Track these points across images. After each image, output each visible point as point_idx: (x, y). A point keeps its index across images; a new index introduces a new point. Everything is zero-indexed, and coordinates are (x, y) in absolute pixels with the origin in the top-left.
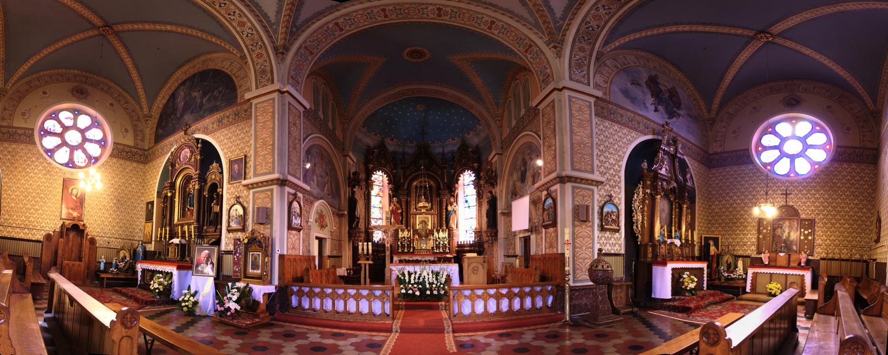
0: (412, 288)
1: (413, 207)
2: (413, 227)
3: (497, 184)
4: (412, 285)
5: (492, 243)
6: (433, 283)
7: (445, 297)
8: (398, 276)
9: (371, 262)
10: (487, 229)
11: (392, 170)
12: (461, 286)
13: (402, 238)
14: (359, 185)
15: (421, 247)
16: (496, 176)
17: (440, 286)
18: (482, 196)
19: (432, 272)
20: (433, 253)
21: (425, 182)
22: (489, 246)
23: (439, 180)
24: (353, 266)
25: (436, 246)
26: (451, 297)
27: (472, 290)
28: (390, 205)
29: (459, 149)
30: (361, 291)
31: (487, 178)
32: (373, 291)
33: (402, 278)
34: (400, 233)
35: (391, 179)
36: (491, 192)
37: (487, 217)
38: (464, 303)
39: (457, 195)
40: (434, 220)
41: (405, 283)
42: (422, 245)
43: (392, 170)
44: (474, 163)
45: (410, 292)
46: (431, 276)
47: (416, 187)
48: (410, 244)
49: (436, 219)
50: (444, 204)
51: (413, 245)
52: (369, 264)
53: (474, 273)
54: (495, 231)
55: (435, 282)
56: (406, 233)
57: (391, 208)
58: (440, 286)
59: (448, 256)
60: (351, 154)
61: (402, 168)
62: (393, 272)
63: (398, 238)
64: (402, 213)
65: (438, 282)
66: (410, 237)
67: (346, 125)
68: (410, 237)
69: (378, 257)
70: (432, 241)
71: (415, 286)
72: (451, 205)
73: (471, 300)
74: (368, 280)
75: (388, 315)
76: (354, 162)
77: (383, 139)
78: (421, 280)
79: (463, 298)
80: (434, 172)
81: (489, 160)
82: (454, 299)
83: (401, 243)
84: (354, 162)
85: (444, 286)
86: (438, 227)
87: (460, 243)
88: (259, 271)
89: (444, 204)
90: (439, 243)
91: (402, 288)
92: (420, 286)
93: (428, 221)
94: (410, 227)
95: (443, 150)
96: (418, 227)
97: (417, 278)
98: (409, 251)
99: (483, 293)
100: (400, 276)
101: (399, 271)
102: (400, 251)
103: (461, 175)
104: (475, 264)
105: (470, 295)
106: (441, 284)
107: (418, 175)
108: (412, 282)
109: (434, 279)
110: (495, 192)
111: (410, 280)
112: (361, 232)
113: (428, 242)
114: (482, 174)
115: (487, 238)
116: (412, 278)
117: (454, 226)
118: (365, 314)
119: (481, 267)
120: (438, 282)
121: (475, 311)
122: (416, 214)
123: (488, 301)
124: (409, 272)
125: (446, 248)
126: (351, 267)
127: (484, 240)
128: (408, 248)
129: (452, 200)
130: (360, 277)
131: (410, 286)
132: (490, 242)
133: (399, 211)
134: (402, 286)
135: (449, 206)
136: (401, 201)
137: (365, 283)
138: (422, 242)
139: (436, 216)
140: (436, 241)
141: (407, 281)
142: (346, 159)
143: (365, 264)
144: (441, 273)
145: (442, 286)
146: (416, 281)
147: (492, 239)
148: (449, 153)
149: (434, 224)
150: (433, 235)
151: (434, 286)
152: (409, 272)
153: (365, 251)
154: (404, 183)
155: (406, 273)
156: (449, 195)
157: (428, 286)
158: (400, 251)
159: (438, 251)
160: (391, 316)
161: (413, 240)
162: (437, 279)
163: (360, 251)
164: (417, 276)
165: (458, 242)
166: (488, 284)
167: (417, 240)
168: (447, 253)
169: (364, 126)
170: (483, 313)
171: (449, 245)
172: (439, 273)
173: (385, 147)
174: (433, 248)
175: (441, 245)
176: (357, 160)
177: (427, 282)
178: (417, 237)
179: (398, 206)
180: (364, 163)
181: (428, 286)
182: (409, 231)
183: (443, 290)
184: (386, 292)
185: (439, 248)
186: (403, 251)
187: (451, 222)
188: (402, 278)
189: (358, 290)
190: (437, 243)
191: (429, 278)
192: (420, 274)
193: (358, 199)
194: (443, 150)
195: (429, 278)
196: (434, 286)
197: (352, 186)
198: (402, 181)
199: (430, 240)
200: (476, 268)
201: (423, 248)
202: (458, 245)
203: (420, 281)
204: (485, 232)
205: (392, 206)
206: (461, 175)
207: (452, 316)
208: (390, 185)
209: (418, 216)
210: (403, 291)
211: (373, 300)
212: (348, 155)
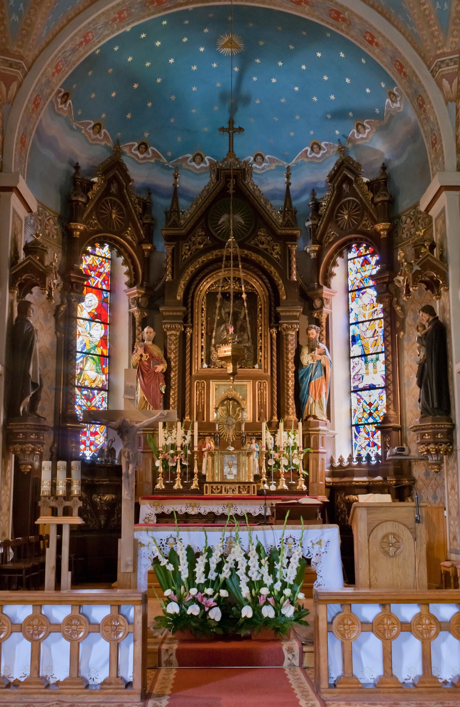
0: (199, 597)
1: (200, 355)
2: (200, 416)
3: (446, 283)
4: (200, 588)
5: (439, 464)
6: (261, 584)
7: (299, 628)
8: (156, 561)
9: (78, 521)
10: (422, 418)
11: (140, 243)
12: (350, 590)
13: (166, 447)
14: (43, 285)
15: (223, 476)
16: (443, 258)
17: (281, 594)
18: (403, 322)
19: (259, 549)
20: (261, 493)
21: (237, 280)
22: (427, 474)
23: (276, 275)
24: (16, 533)
25: (268, 474)
26: (323, 625)
27: (384, 604)
28: (132, 349)
29: (332, 178)
30: (46, 609)
31: (417, 268)
32: (85, 609)
33: (170, 567)
34: (162, 432)
35: (135, 269)
36: (429, 310)
37: (420, 384)
38: (360, 646)
39: (327, 319)
40: (262, 394)
41: (180, 583)
42: (226, 469)
43: (140, 243)
44: (376, 222)
45: (194, 610)
46: (253, 562)
47: (211, 296)
48: (191, 466)
49: (267, 393)
50: (292, 347)
51: (200, 468)
52: (71, 526)
53: (386, 553)
54: (447, 425)
55: (268, 580)
56: (179, 431)
57: (136, 357)
58: (281, 594)
59: (305, 500)
60: (22, 186)
61: (169, 239)
62: (143, 551)
63: (156, 448)
64: (167, 375)
65: (275, 581)
66: (191, 446)
67: (14, 85)
68: (191, 446)
69: (94, 504)
70: (254, 457)
71: (209, 591)
72: (312, 350)
73: (381, 635)
74: (66, 576)
75: (129, 685)
76: (30, 210)
77: (117, 143)
78: (226, 574)
79: (357, 628)
80: (258, 251)
81: (422, 208)
82: (329, 631)
83: (165, 461)
84: (30, 210)
85: (294, 593)
86: (272, 415)
87: (337, 464)
88: (344, 172)
89: (292, 347)
90: (277, 463)
91: (169, 600)
92: (224, 593)
93: (244, 399)
94: (191, 414)
95: (289, 184)
96: (213, 416)
97: (213, 566)
98: (187, 486)
99: (419, 617)
100: (164, 562)
101: (161, 548)
102: (160, 485)
103: (339, 260)
104: (388, 528)
105: (379, 620)
106: (284, 585)
107: (219, 260)
108: (200, 579)
109: (265, 570)
110: (444, 309)
111: (192, 575)
112: (43, 428)
113: (244, 459)
114: (400, 255)
115: (422, 448)
116: (200, 569)
117: (321, 414)
118: (58, 683)
119: (406, 535)
120: (275, 581)
121: (395, 672)
122: (208, 378)
123: (434, 643)
124: (189, 549)
125: (296, 479)
126: (9, 537)
127: (414, 454)
128: (183, 478)
129: (314, 333)
130: (43, 565)
131: (194, 591)
132: (432, 459)
133: (161, 368)
134: (168, 592)
135: (305, 351)
136: (165, 337)
137: (58, 585)
138: (227, 458)
139: (267, 384)
140: (268, 457)
141: (185, 575)
142: (8, 200)
143: (60, 528)
144: (285, 554)
145: (287, 592)
146: (212, 576)
147: (437, 452)
148: (303, 192)
149: (262, 406)
150: (259, 438)
151: (264, 591)
152: (189, 549)
153: (61, 490)
154: (174, 284)
155: (182, 554)
156: (304, 319)
157: (245, 592)
158: (160, 485)
159: (273, 488)
160: (138, 686)
161: (201, 454)
162: (272, 571)
163: (45, 487)
164: (214, 561)
165: (332, 461)
166: (429, 588)
167: (211, 454)
168: (302, 493)
169: (66, 96)
170: (421, 679)
171: (307, 468)
172: (279, 552)
173: (123, 170)
174: (257, 478)
175: (282, 470)
176: (41, 205)
177: (244, 580)
178: (210, 444)
179: (157, 351)
180: (61, 218)
181: (245, 592)
182: (187, 427)
183: (292, 603)
184: (124, 609)
185: (277, 478)
186: (169, 486)
187: (311, 400)
188: (170, 567)
189: (37, 605)
190: (271, 462)
191: (248, 568)
192: (224, 556)
193: (36, 326)
194: (289, 184)
195: (248, 568)
196: (264, 591)
197: (21, 286)
198: (169, 278)
199: (249, 454)
200: (392, 539)
201: (230, 478)
202: (332, 467)
203: (222, 577)
204: (416, 429)
205: (140, 351)
206: (339, 260)
207: (324, 685)
208: (135, 290)
209: (213, 384)
210: (173, 608)
211: (85, 637)
212: (12, 189)
